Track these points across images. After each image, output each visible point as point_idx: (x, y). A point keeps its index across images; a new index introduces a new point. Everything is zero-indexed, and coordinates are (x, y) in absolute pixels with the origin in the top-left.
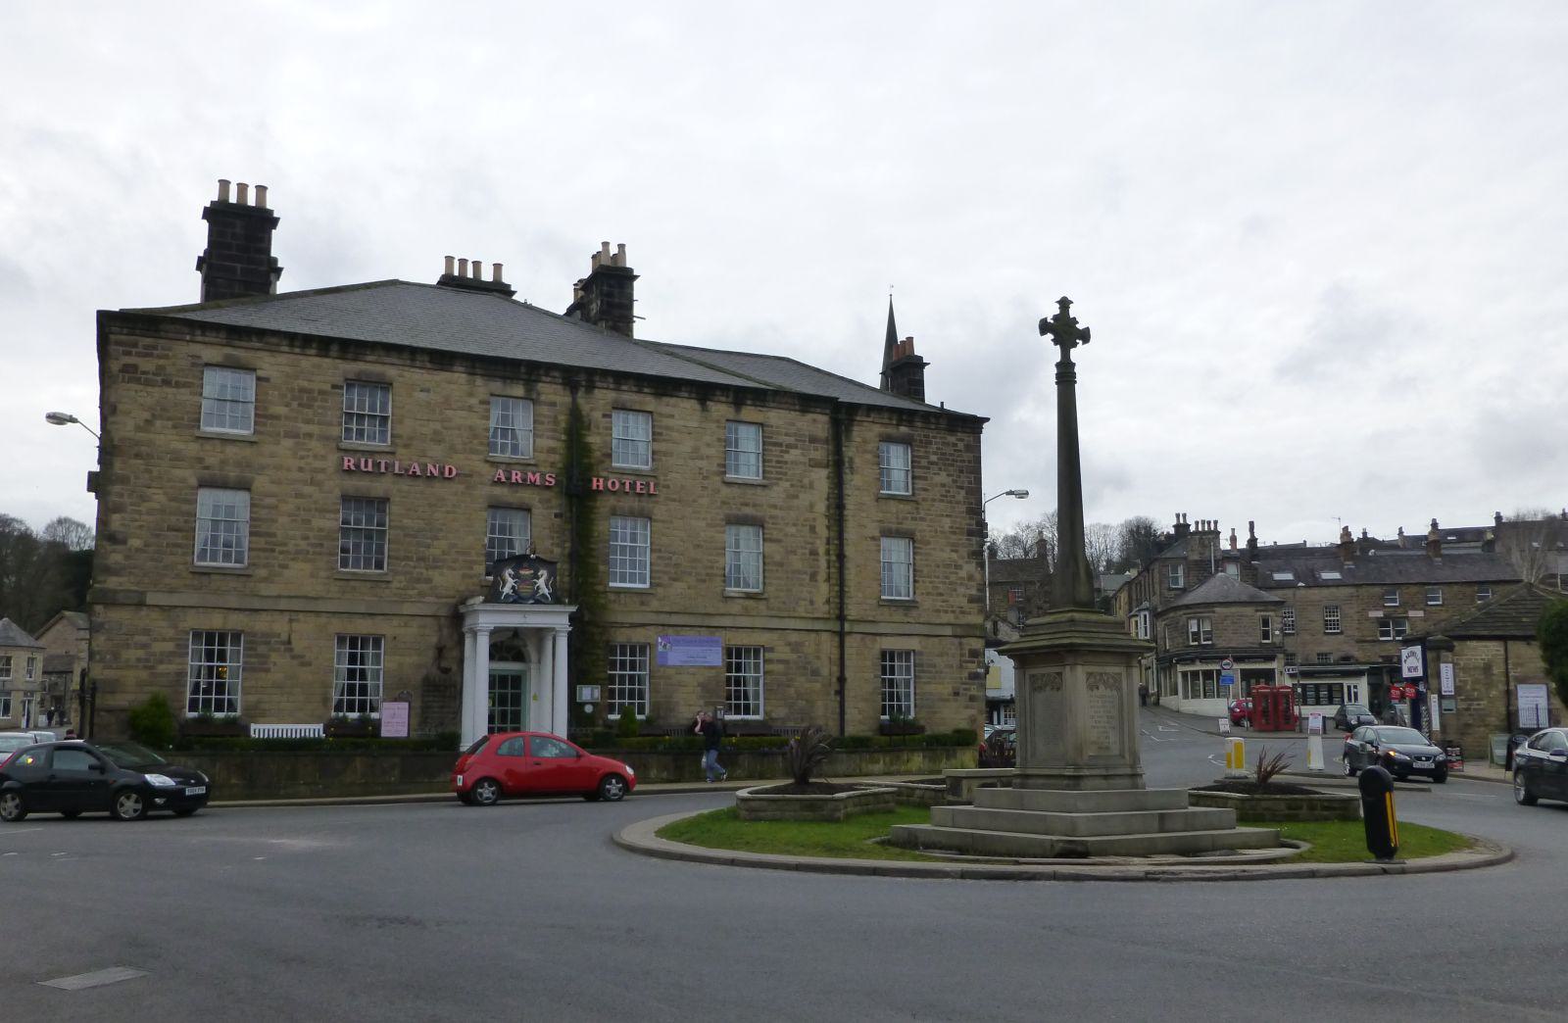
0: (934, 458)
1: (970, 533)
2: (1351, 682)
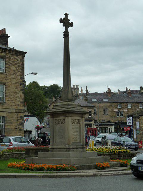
0: (11, 62)
1: (21, 84)
2: (109, 127)
